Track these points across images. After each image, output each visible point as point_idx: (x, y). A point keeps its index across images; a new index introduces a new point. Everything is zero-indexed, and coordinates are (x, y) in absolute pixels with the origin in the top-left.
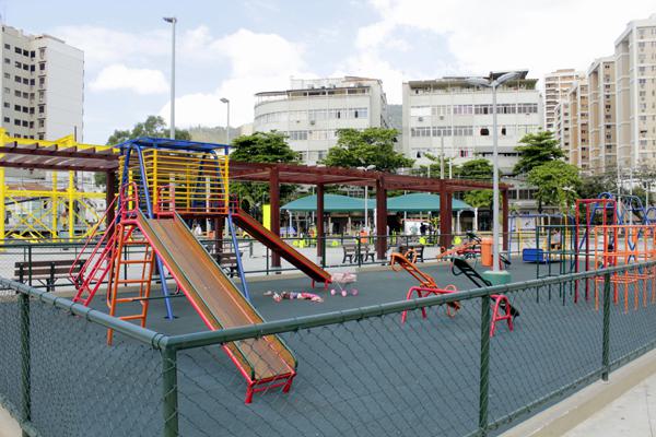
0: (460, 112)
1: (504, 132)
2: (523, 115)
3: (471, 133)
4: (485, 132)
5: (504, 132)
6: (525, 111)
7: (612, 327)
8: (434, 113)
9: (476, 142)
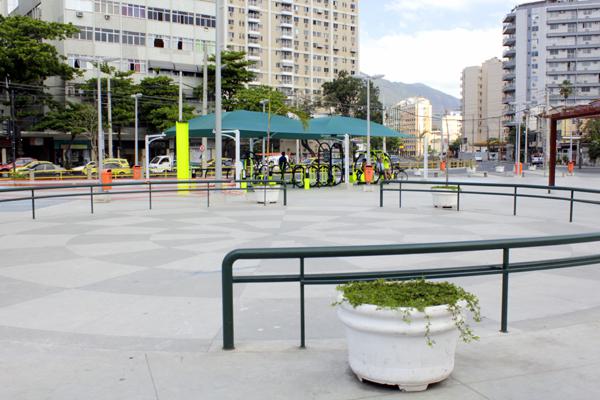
0: (131, 14)
1: (180, 46)
2: (201, 28)
3: (143, 42)
4: (159, 43)
5: (180, 46)
6: (203, 25)
7: (299, 313)
8: (97, 10)
9: (148, 54)
